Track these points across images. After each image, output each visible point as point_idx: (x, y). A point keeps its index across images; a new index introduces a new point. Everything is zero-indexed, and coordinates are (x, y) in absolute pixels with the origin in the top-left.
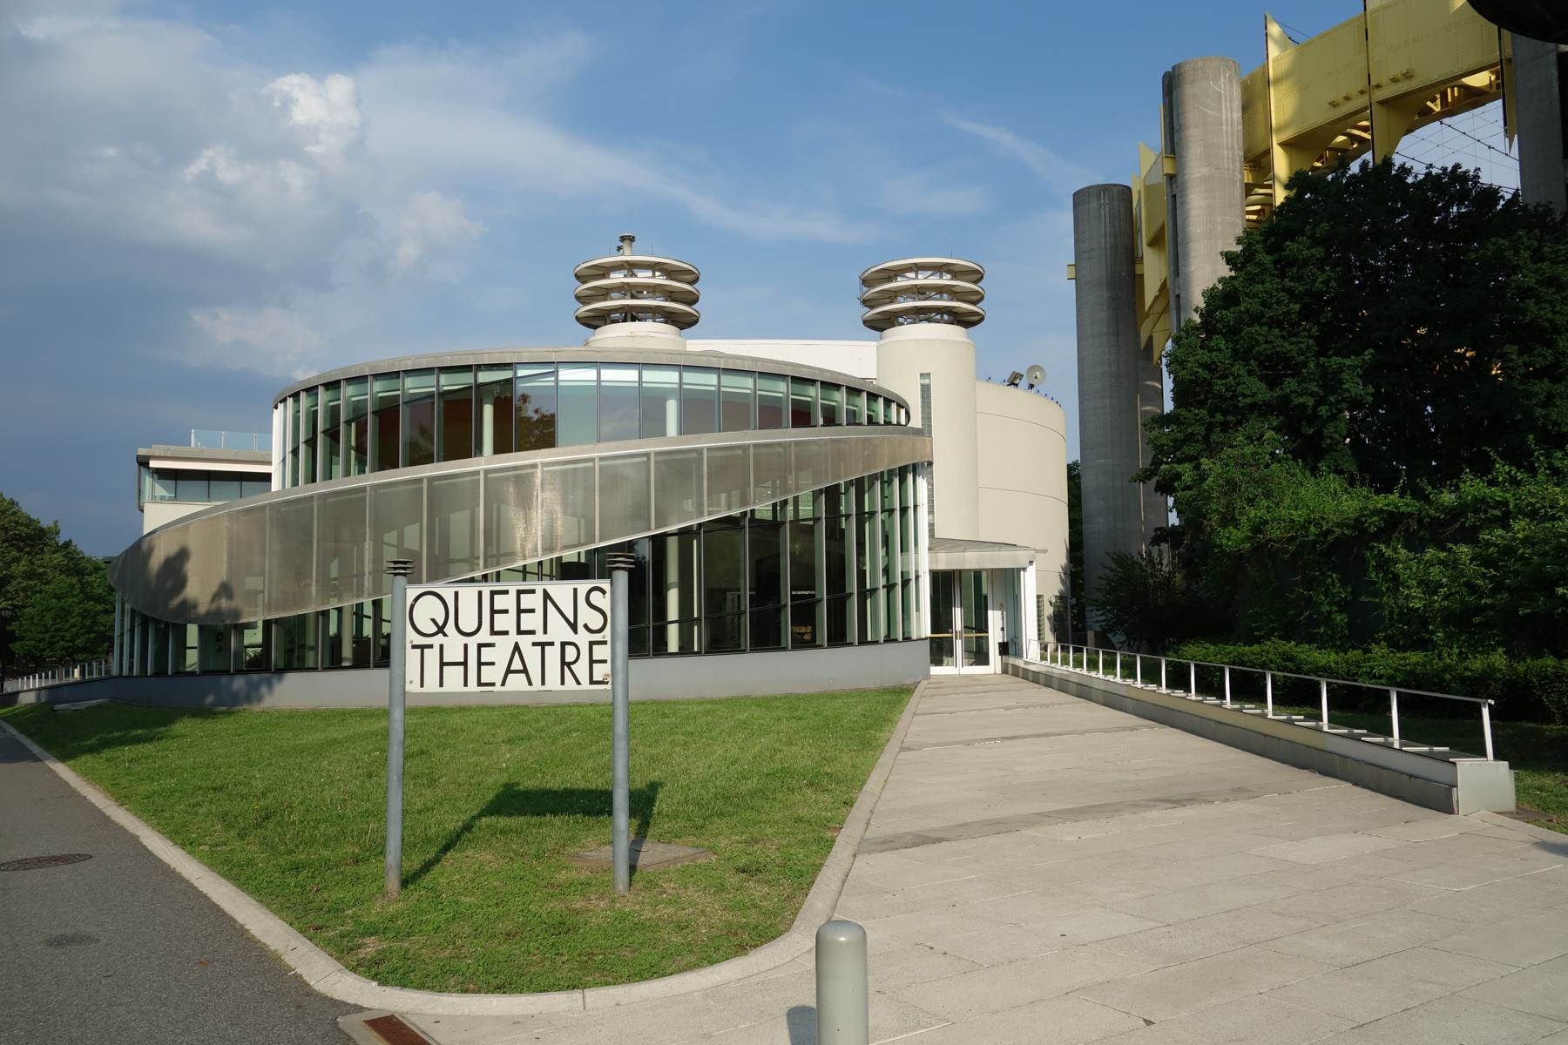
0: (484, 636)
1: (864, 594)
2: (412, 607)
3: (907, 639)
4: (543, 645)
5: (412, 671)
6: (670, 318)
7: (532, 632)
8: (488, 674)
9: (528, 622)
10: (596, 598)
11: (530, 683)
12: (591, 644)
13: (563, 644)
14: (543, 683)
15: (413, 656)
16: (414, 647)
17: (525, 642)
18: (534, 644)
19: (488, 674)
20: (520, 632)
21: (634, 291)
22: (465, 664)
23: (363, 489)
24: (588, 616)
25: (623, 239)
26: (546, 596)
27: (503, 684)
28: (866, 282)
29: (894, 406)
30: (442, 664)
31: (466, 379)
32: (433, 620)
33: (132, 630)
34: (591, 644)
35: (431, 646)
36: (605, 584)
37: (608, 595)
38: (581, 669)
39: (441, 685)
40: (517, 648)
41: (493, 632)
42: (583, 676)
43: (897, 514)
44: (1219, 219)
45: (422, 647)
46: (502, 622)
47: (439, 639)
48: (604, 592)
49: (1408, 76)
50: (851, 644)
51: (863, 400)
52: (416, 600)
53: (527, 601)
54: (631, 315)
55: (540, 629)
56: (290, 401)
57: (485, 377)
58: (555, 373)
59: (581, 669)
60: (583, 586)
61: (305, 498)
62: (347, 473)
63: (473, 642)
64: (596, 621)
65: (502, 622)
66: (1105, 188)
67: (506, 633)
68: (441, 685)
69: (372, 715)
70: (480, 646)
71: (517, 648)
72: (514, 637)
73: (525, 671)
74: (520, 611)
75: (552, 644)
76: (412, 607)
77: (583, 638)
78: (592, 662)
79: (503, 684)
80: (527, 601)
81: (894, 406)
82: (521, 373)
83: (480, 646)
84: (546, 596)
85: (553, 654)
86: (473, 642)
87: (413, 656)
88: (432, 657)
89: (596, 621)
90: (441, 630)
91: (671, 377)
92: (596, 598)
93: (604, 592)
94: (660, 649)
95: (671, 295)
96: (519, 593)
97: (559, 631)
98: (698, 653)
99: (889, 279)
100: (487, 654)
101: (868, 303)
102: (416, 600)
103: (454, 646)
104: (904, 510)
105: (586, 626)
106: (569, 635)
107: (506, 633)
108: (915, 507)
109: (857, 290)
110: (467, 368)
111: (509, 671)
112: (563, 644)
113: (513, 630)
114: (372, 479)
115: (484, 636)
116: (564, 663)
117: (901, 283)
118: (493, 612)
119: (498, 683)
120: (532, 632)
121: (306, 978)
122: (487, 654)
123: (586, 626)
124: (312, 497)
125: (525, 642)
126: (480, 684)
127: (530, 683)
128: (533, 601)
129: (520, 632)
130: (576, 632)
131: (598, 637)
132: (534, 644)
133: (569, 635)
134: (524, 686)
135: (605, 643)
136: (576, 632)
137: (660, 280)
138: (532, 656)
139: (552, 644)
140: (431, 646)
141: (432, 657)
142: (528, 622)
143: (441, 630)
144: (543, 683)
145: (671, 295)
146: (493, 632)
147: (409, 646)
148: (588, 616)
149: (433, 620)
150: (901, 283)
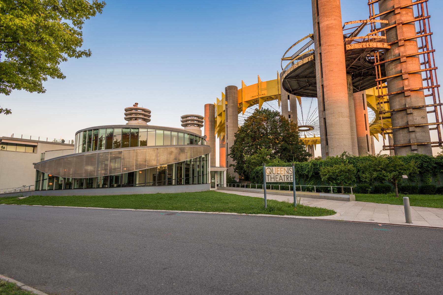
1: (43, 180)
3: (206, 183)
17: (282, 175)
23: (96, 154)
25: (136, 104)
28: (126, 110)
36: (292, 168)
38: (289, 179)
47: (270, 175)
49: (284, 72)
59: (289, 179)
60: (289, 168)
62: (93, 150)
66: (210, 105)
77: (289, 175)
85: (286, 177)
86: (275, 175)
87: (267, 177)
88: (269, 177)
90: (270, 173)
91: (161, 132)
94: (61, 189)
95: (199, 121)
98: (175, 185)
100: (277, 177)
109: (180, 119)
114: (94, 152)
115: (276, 174)
117: (189, 118)
121: (384, 194)
122: (277, 177)
137: (197, 119)
141: (269, 177)
145: (199, 121)
148: (290, 172)
150: (189, 118)
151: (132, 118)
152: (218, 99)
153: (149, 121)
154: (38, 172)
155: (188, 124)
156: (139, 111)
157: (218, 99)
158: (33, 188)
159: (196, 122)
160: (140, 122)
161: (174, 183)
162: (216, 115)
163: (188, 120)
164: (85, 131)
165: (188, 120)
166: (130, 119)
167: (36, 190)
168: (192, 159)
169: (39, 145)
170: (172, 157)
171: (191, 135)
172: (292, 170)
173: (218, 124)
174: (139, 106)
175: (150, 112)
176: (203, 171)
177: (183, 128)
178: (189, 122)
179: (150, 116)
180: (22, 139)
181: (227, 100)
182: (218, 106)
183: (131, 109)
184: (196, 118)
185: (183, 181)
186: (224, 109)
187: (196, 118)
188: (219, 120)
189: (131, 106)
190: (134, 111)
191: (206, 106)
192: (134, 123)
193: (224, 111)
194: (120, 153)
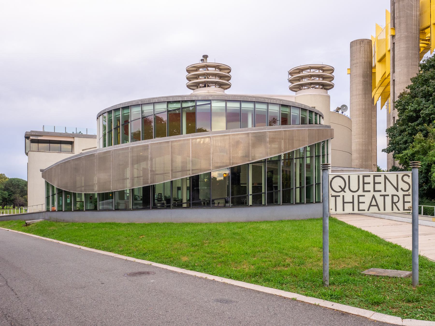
0: (360, 192)
2: (331, 181)
4: (384, 196)
5: (332, 205)
6: (221, 85)
7: (380, 191)
8: (362, 206)
9: (378, 187)
10: (406, 178)
11: (379, 210)
12: (404, 195)
13: (393, 196)
14: (385, 210)
15: (332, 200)
16: (332, 196)
17: (377, 195)
18: (381, 195)
19: (362, 206)
20: (375, 191)
21: (206, 75)
22: (353, 202)
24: (402, 185)
25: (204, 56)
26: (386, 178)
27: (368, 210)
28: (291, 74)
29: (318, 116)
30: (344, 203)
31: (178, 106)
32: (340, 186)
33: (53, 195)
34: (404, 195)
35: (339, 196)
36: (409, 173)
37: (411, 177)
38: (400, 205)
39: (344, 210)
40: (374, 197)
41: (364, 191)
42: (401, 208)
43: (321, 157)
44: (410, 52)
45: (336, 196)
46: (367, 187)
48: (409, 176)
50: (312, 203)
51: (308, 114)
52: (333, 179)
53: (377, 179)
54: (206, 85)
55: (383, 190)
56: (106, 115)
57: (185, 105)
58: (210, 104)
60: (400, 174)
61: (126, 148)
63: (356, 195)
64: (406, 187)
65: (367, 187)
66: (362, 41)
67: (369, 191)
68: (344, 210)
69: (251, 222)
70: (359, 196)
71: (374, 197)
72: (372, 193)
73: (377, 205)
74: (375, 183)
75: (388, 195)
76: (331, 181)
77: (401, 194)
78: (404, 202)
79: (368, 210)
80: (377, 179)
81: (318, 116)
82: (198, 103)
83: (359, 196)
84: (386, 178)
85: (388, 200)
87: (332, 200)
88: (340, 200)
89: (406, 187)
90: (343, 190)
91: (251, 106)
92: (406, 178)
93: (409, 176)
95: (221, 77)
96: (374, 176)
97: (391, 190)
99: (299, 73)
101: (291, 81)
102: (333, 179)
103: (348, 196)
104: (323, 156)
105: (402, 189)
106: (395, 192)
107: (369, 191)
108: (327, 154)
109: (287, 77)
110: (179, 102)
111: (370, 205)
112: (393, 196)
113: (372, 190)
115: (360, 192)
116: (393, 202)
117: (305, 73)
118: (364, 183)
119: (366, 209)
120: (380, 191)
123: (402, 189)
124: (128, 148)
125: (377, 195)
126: (359, 210)
127: (379, 210)
128: (381, 179)
129: (375, 191)
130: (398, 191)
131: (407, 193)
132: (381, 195)
133: (395, 192)
134: (377, 211)
135: (409, 195)
136: (398, 191)
138: (380, 200)
139: (388, 195)
140: (339, 196)
141: (340, 200)
142: (378, 187)
143: (343, 190)
144: (385, 210)
145: (221, 77)
146: (364, 191)
147: (330, 196)
148: (402, 185)
149: (340, 186)
150: (305, 73)
151: (199, 83)
152: (377, 27)
153: (229, 86)
154: (47, 184)
155: (302, 85)
156: (211, 70)
157: (377, 27)
158: (44, 209)
159: (317, 80)
160: (213, 90)
161: (250, 203)
162: (375, 61)
163: (302, 77)
164: (110, 112)
165: (302, 77)
166: (197, 86)
167: (48, 210)
168: (282, 154)
169: (77, 141)
170: (240, 153)
171: (283, 105)
172: (409, 180)
173: (378, 78)
174: (210, 61)
175: (332, 70)
176: (228, 186)
177: (189, 92)
178: (305, 81)
179: (332, 78)
180: (54, 133)
181: (394, 26)
182: (379, 41)
183: (197, 68)
184: (317, 72)
185: (264, 199)
186: (389, 47)
187: (317, 72)
188: (379, 71)
189: (197, 61)
190: (201, 71)
191: (352, 44)
192: (202, 92)
193: (389, 51)
194: (146, 148)
